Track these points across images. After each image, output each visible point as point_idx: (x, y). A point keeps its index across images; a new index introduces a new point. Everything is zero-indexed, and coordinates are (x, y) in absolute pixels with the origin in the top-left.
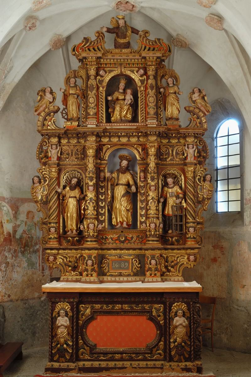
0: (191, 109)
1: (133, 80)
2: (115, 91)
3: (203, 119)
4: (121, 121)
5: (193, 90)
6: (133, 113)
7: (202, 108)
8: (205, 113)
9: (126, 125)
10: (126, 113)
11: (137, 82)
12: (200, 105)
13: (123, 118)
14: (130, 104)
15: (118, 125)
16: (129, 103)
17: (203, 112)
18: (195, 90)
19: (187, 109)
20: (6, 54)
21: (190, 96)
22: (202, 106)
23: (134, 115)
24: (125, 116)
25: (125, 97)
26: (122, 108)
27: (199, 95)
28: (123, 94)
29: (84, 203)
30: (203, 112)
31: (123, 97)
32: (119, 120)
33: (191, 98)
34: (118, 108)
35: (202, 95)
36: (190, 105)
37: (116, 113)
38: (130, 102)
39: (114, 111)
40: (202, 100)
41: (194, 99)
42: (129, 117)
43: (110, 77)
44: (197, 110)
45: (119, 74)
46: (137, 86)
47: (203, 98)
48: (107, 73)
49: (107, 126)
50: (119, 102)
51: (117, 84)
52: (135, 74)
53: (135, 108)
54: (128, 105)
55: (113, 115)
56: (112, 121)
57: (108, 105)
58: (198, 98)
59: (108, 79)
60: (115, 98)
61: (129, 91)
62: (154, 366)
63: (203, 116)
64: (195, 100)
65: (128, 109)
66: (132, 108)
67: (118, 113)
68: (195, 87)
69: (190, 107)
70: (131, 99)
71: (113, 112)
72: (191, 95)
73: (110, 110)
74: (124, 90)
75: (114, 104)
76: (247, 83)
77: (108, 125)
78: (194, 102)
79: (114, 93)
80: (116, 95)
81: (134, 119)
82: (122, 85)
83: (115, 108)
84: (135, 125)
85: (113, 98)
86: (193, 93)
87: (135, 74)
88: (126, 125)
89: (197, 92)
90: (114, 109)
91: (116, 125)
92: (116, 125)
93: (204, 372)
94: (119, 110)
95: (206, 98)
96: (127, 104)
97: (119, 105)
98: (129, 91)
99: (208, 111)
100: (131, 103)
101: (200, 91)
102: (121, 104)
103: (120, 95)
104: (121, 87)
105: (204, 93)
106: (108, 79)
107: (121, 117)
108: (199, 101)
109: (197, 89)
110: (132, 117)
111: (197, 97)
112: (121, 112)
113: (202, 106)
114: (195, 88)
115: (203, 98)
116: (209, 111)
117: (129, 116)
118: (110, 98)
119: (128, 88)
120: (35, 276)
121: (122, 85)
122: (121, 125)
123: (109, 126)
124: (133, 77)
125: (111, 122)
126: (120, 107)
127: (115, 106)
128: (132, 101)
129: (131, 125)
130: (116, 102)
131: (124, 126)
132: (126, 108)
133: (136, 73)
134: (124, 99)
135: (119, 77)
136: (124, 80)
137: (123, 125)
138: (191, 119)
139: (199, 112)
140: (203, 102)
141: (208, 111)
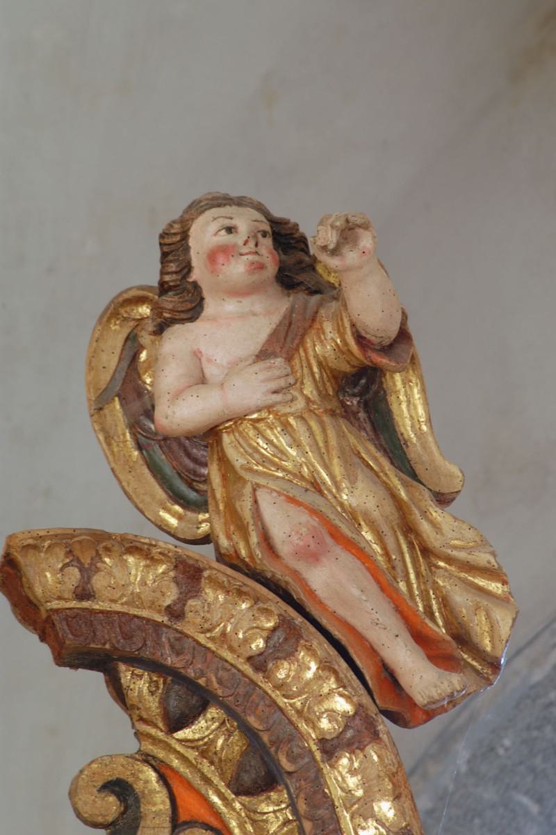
0: (134, 583)
3: (345, 777)
5: (174, 247)
7: (333, 581)
8: (390, 678)
12: (285, 524)
17: (345, 651)
18: (205, 235)
19: (50, 579)
20: (490, 582)
21: (111, 359)
22: (337, 533)
27: (285, 342)
29: (346, 693)
30: (345, 651)
33: (129, 390)
35: (326, 344)
36: (117, 517)
40: (335, 432)
41: (181, 412)
44: (234, 622)
47: (359, 392)
58: (249, 389)
63: (356, 734)
64: (211, 434)
68: (198, 193)
69: (100, 542)
72: (132, 344)
76: (356, 674)
78: (186, 462)
86: (179, 298)
89: (237, 269)
93: (498, 655)
95: (410, 405)
99: (451, 646)
101: (293, 262)
105: (370, 303)
108: (290, 461)
109: (245, 221)
111: (234, 367)
113: (337, 533)
114: (197, 208)
115: (359, 392)
116: (463, 638)
138: (120, 788)
139: (284, 643)
140: (352, 459)
141: (451, 646)
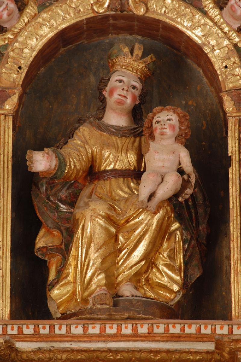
1: (197, 52)
2: (81, 121)
4: (116, 306)
6: (195, 262)
9: (143, 330)
10: (150, 259)
11: (218, 66)
13: (127, 290)
14: (173, 200)
15: (94, 329)
16: (165, 191)
23: (196, 274)
24: (138, 274)
25: (140, 157)
26: (119, 228)
28: (129, 141)
31: (132, 157)
32: (100, 299)
34: (92, 224)
37: (81, 252)
38: (170, 185)
39: (68, 249)
42: (165, 280)
43: (47, 33)
45: (105, 18)
46: (218, 89)
48: (31, 10)
49: (20, 336)
50: (103, 187)
51: (92, 79)
52: (205, 14)
53: (203, 227)
54: (159, 207)
55: (60, 272)
56: (52, 307)
57: (31, 207)
59: (33, 42)
60: (75, 162)
61: (167, 121)
62: (214, 57)
65: (162, 233)
66: (185, 226)
67: (93, 255)
70: (181, 171)
71: (65, 250)
73: (41, 241)
74: (139, 113)
75: (72, 203)
77: (28, 330)
79: (71, 135)
80: (83, 144)
81: (204, 295)
82: (124, 81)
83: (76, 224)
84: (206, 330)
85: (62, 162)
87: (205, 14)
88: (143, 330)
90: (69, 230)
91: (77, 330)
92: (77, 330)
94: (100, 237)
96: (151, 197)
97: (101, 208)
98: (167, 121)
100: (176, 195)
102: (112, 202)
103: (105, 145)
104: (116, 96)
106: (33, 42)
107: (112, 284)
110: (184, 285)
112: (113, 251)
117: (168, 279)
118: (41, 162)
119: (164, 102)
120: (87, 131)
121: (124, 81)
122: (111, 329)
123: (36, 336)
124: (196, 35)
125: (46, 315)
126: (108, 219)
127: (78, 213)
128: (185, 184)
129: (175, 329)
130: (86, 191)
131: (135, 336)
132: (148, 222)
133: (214, 12)
134: (136, 174)
135: (107, 40)
136: (138, 52)
137: (127, 329)
